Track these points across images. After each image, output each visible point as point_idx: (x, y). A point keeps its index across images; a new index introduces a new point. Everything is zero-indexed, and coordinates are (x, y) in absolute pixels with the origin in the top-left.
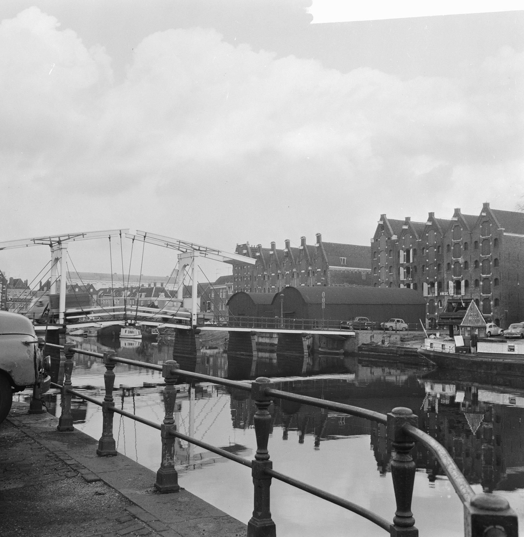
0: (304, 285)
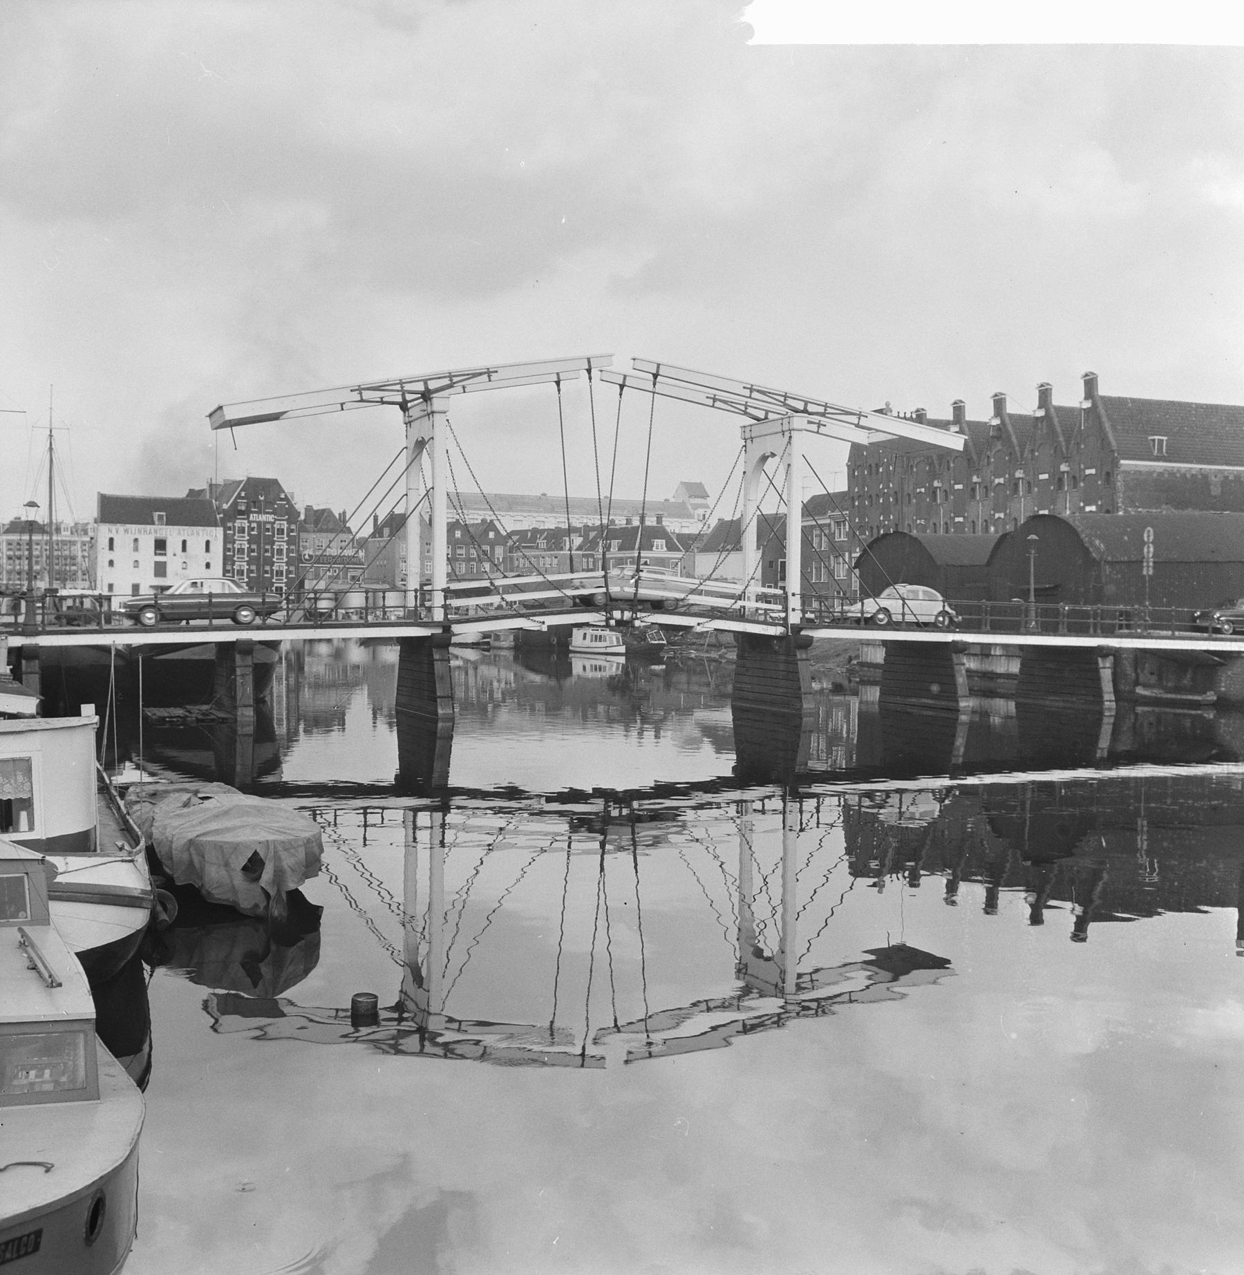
0: (1093, 508)
